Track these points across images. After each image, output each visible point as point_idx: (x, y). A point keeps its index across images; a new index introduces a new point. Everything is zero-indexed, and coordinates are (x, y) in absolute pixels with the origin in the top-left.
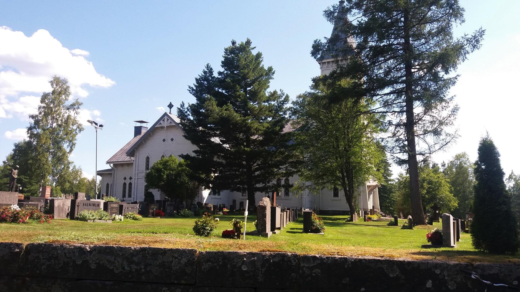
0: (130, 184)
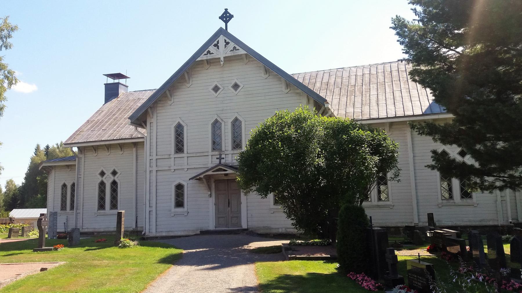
0: (114, 183)
